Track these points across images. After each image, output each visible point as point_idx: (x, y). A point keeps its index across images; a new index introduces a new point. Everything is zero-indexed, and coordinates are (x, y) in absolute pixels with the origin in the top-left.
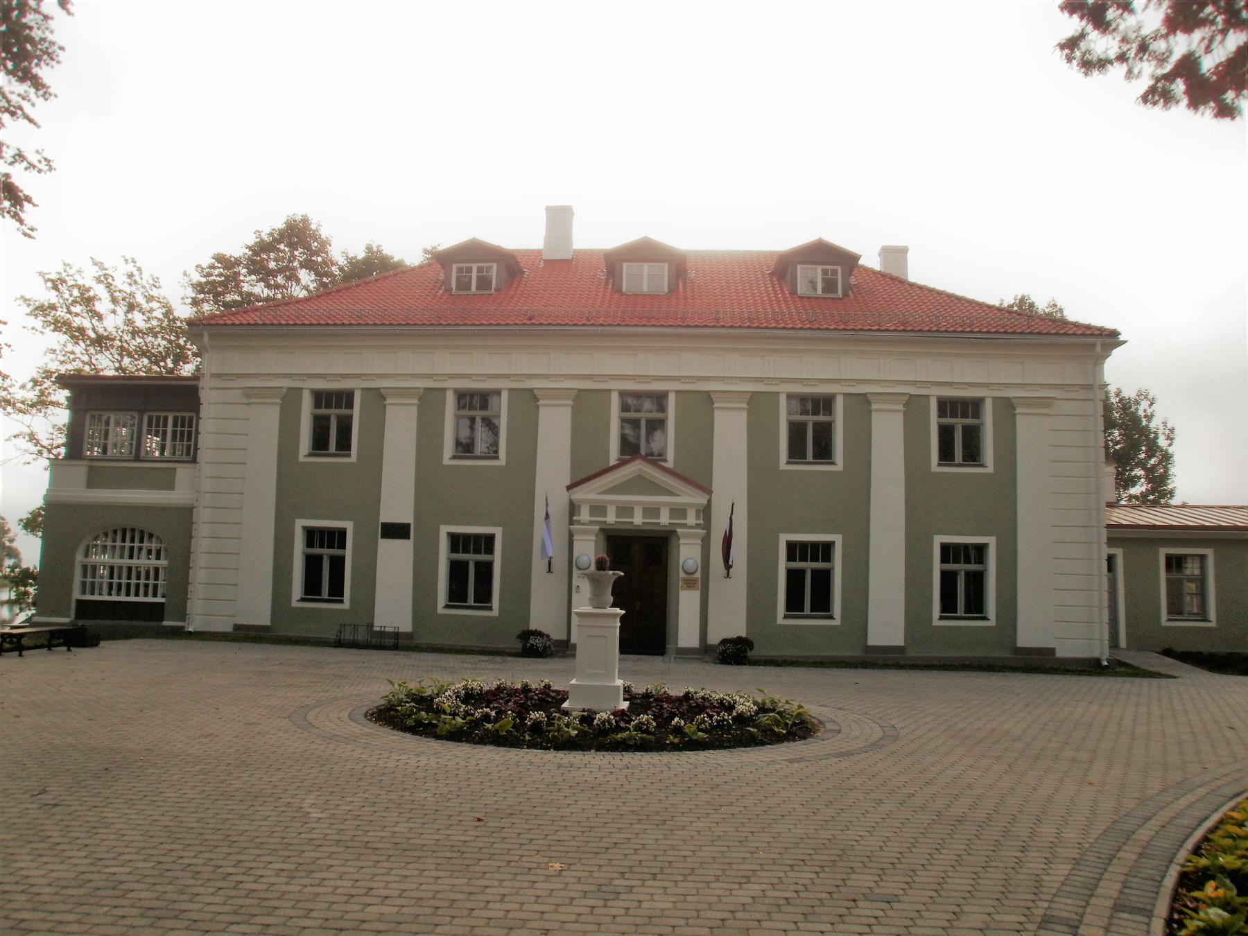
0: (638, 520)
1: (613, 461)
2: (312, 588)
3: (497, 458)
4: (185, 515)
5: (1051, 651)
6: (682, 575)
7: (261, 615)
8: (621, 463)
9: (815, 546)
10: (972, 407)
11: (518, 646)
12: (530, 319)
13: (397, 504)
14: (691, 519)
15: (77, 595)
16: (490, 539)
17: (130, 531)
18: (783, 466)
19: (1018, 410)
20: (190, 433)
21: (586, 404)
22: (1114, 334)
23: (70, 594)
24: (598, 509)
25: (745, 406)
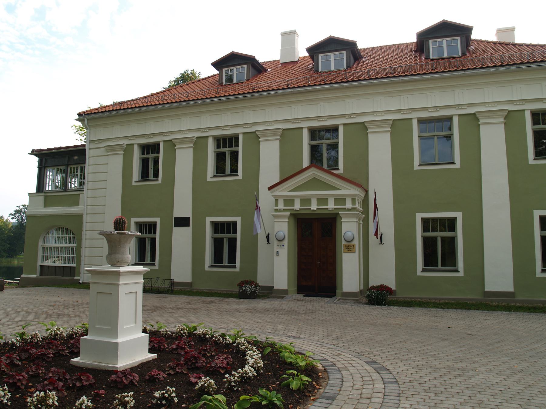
0: (314, 207)
2: (218, 259)
4: (79, 217)
6: (344, 242)
9: (442, 221)
11: (236, 289)
13: (183, 207)
15: (40, 263)
21: (288, 137)
24: (289, 201)
25: (389, 129)
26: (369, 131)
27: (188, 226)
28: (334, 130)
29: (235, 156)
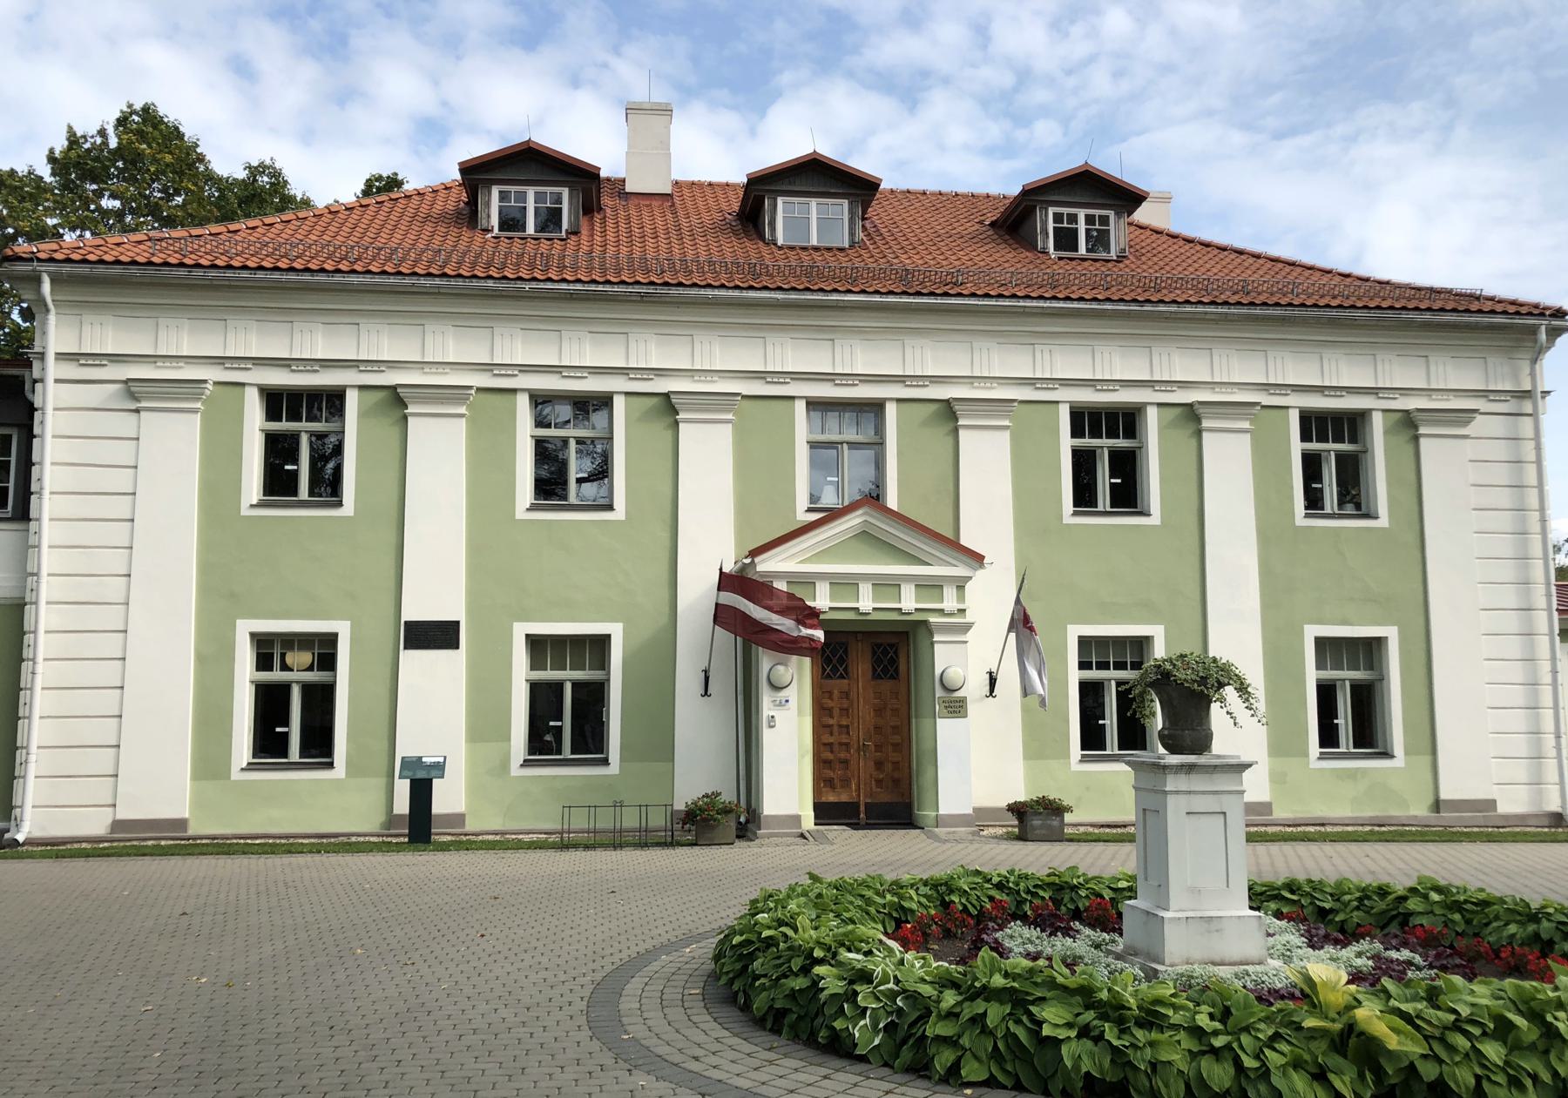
0: (866, 602)
3: (610, 507)
6: (939, 693)
9: (578, 641)
10: (1125, 420)
12: (756, 276)
16: (602, 642)
19: (1422, 430)
27: (455, 645)
28: (333, 400)
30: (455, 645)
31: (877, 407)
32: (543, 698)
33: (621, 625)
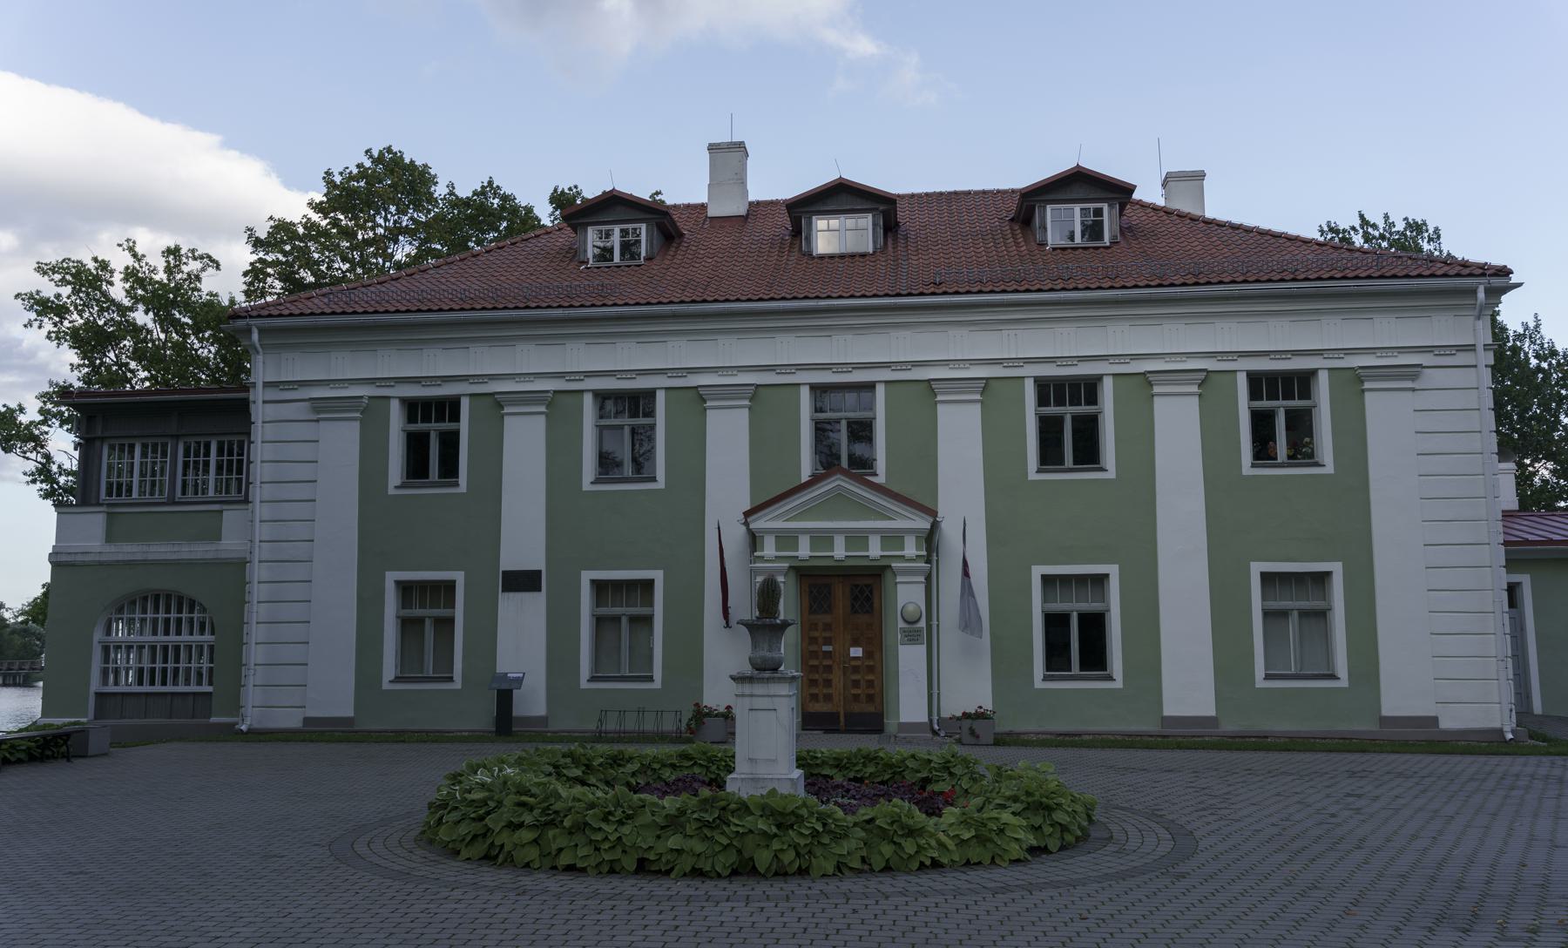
0: (839, 551)
1: (805, 476)
4: (237, 568)
5: (1434, 720)
7: (338, 702)
8: (815, 480)
9: (1081, 579)
14: (911, 549)
15: (95, 685)
17: (163, 600)
18: (1033, 475)
20: (240, 462)
22: (1504, 272)
23: (88, 684)
26: (939, 398)
29: (450, 443)
30: (536, 587)
31: (871, 386)
32: (1055, 624)
33: (1034, 568)
